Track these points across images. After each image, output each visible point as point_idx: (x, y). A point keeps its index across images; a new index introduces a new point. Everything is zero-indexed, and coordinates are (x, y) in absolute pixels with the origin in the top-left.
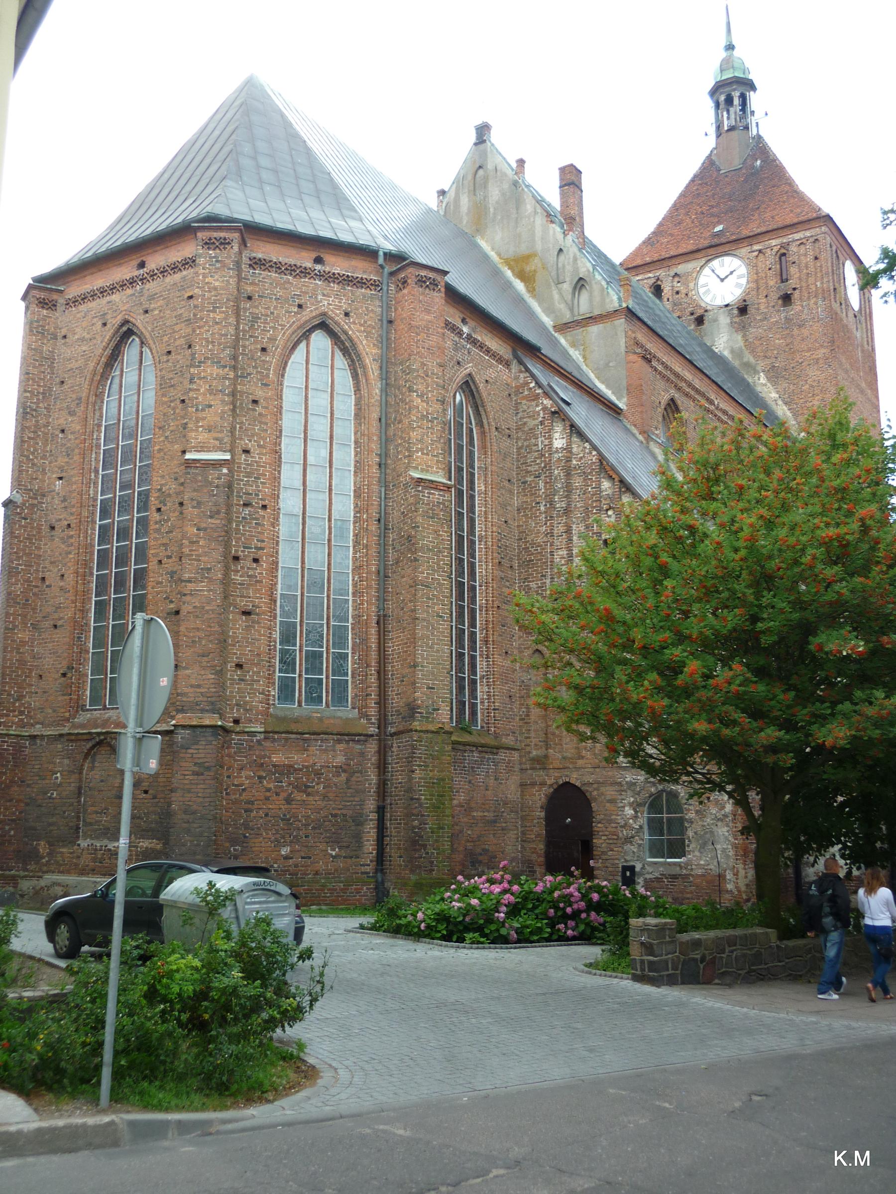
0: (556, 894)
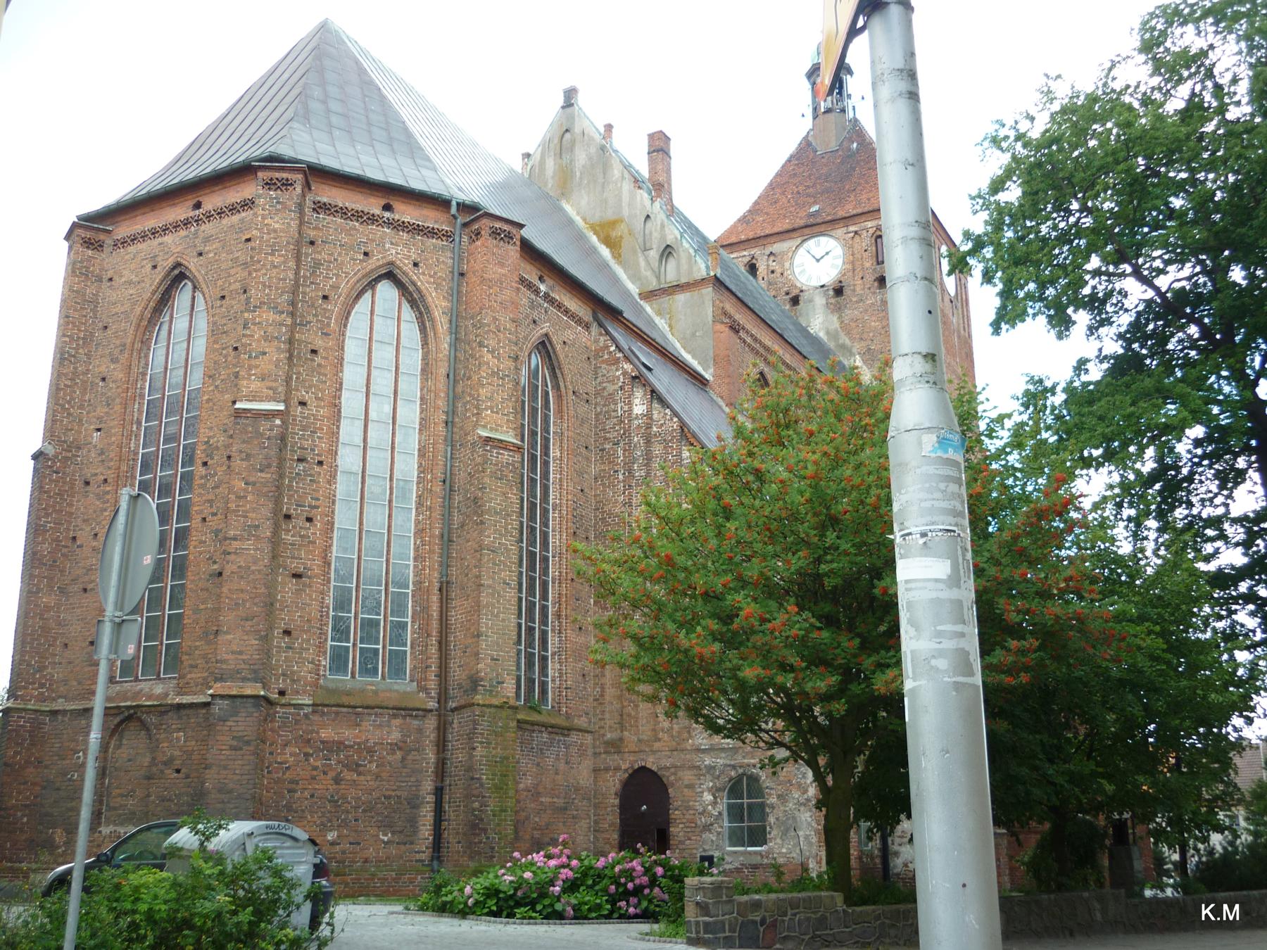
0: (617, 869)
